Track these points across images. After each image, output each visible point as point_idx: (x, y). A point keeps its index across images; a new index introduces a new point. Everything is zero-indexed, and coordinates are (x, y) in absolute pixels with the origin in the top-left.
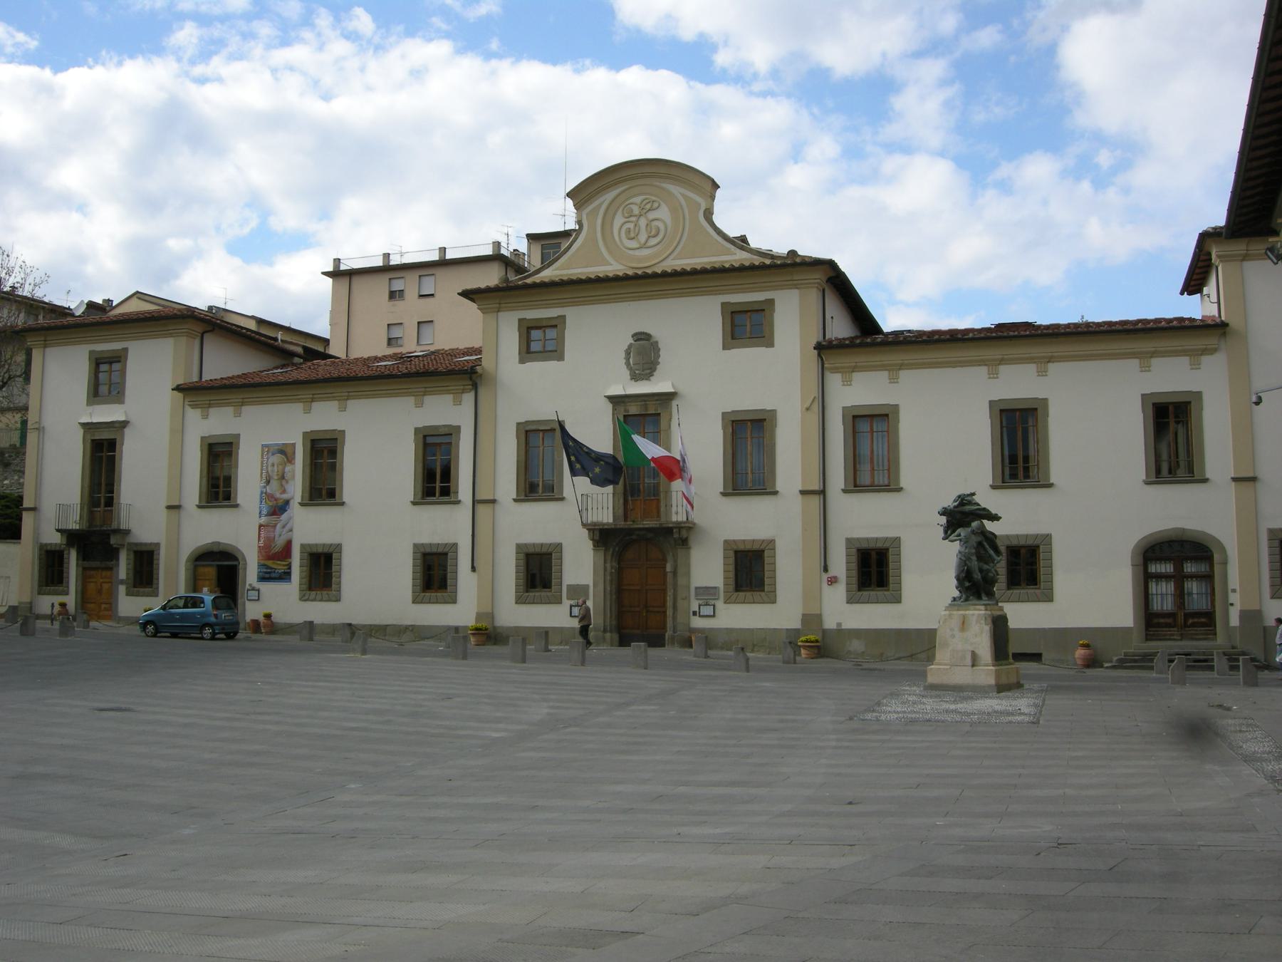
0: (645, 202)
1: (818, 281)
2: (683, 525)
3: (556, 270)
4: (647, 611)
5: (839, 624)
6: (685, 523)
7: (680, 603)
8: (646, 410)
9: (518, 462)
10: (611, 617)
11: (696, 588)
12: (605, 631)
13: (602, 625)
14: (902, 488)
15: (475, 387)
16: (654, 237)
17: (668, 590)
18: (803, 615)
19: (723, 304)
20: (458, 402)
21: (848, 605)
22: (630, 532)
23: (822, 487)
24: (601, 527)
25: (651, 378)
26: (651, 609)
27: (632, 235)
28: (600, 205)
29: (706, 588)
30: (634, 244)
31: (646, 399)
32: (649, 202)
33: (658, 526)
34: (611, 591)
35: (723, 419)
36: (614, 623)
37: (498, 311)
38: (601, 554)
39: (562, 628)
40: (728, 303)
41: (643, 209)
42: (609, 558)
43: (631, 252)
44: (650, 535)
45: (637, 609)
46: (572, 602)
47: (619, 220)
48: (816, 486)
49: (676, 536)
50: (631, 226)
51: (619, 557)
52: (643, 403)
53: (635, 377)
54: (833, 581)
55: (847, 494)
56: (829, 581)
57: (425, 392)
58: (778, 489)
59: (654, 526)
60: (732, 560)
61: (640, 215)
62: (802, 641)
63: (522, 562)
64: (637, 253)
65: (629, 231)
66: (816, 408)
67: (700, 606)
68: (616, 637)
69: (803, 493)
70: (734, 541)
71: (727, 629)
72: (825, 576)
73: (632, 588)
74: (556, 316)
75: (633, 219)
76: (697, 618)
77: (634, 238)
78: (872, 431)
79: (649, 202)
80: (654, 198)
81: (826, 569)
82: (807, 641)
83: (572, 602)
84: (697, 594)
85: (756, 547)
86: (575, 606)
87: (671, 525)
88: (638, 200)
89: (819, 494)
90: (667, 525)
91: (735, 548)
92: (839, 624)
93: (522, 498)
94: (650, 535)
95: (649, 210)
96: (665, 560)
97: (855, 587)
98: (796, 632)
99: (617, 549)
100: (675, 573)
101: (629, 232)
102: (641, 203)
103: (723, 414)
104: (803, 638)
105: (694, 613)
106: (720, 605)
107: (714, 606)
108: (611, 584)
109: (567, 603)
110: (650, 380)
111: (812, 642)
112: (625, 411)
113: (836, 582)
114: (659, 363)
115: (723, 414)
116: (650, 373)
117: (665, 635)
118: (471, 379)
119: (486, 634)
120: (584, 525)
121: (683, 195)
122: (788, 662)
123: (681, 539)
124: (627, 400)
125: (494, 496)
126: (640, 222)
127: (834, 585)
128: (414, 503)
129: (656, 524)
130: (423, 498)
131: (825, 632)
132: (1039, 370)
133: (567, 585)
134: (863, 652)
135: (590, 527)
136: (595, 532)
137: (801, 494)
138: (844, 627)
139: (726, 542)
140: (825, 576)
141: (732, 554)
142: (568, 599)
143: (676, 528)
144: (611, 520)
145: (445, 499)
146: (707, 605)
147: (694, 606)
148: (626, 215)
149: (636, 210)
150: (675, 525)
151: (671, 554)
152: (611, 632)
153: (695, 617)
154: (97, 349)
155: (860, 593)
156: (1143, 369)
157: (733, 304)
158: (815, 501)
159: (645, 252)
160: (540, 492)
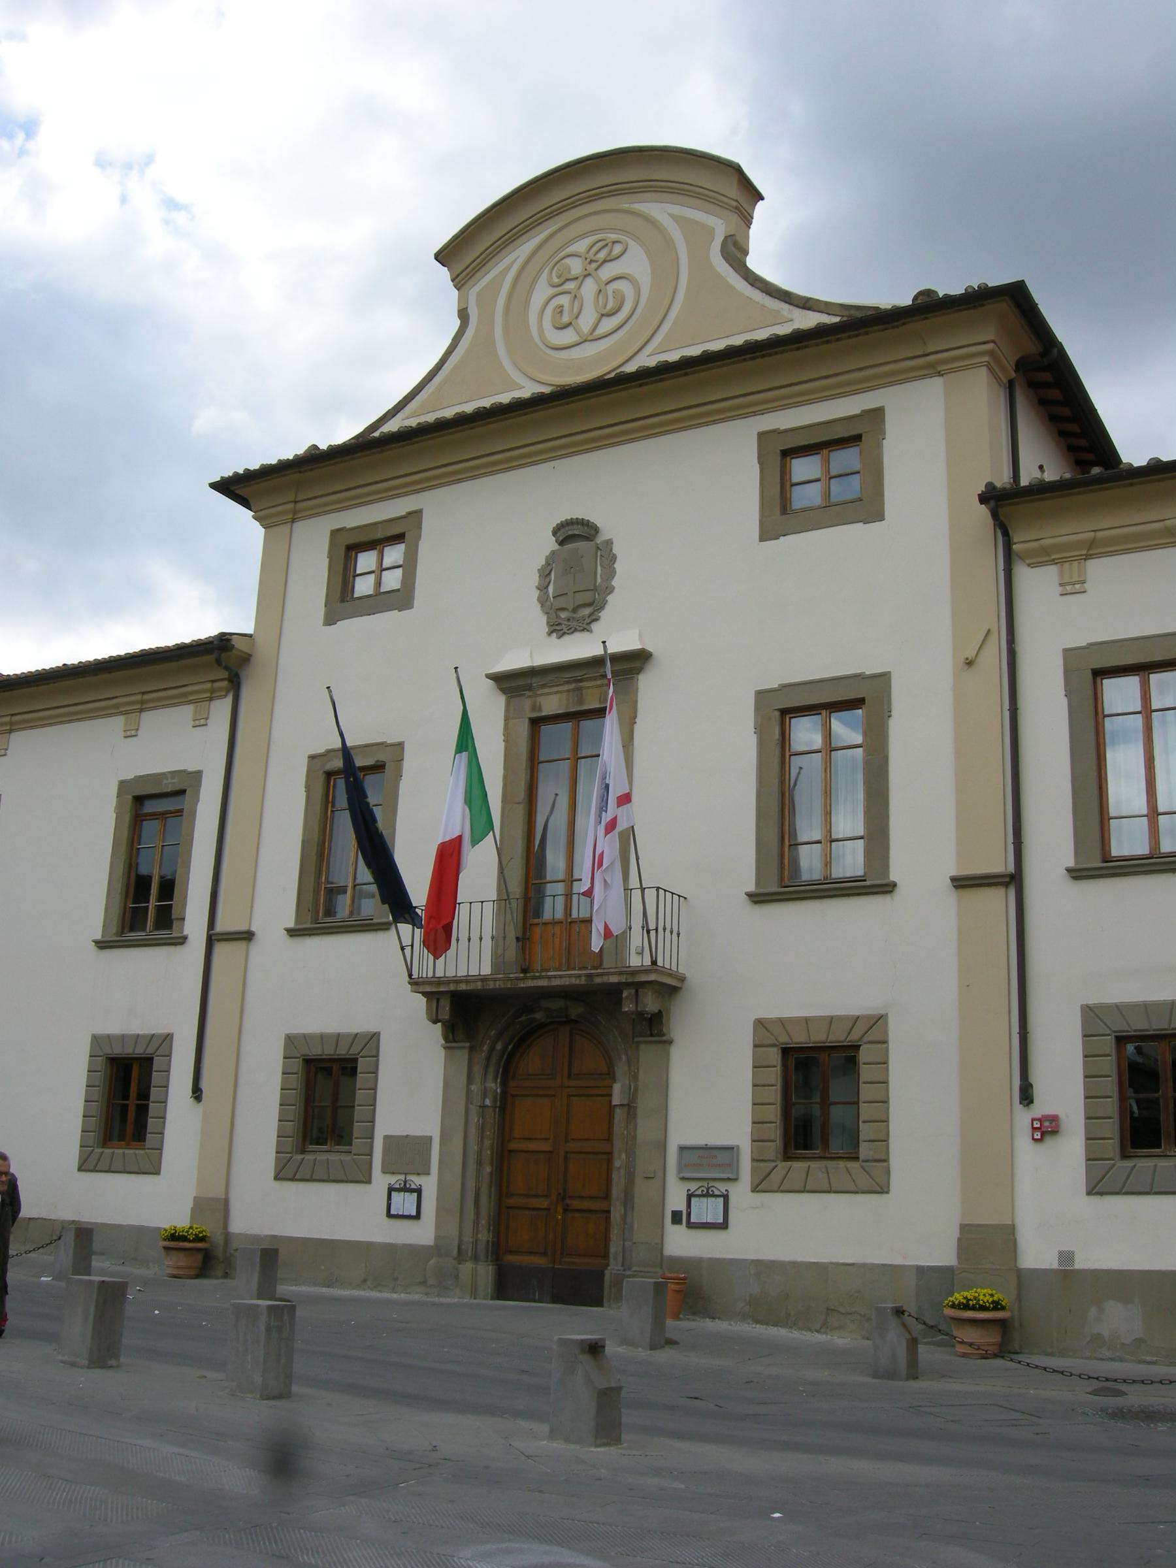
0: (594, 249)
1: (991, 346)
2: (643, 978)
3: (408, 418)
4: (566, 1210)
5: (1066, 1257)
6: (647, 971)
7: (641, 1187)
8: (581, 700)
9: (305, 843)
10: (477, 1220)
11: (682, 1149)
12: (461, 1256)
13: (456, 1243)
14: (894, 885)
15: (235, 684)
16: (609, 315)
17: (616, 1155)
18: (964, 1228)
19: (763, 436)
20: (201, 722)
21: (1092, 1198)
22: (528, 1000)
23: (1011, 868)
24: (452, 987)
25: (594, 626)
26: (575, 1204)
27: (566, 319)
28: (509, 268)
29: (706, 1148)
30: (569, 337)
31: (577, 674)
32: (607, 245)
33: (583, 981)
34: (480, 1152)
35: (758, 707)
36: (484, 1236)
37: (293, 521)
38: (463, 1056)
39: (369, 1245)
40: (774, 431)
41: (591, 261)
42: (478, 1069)
43: (563, 355)
44: (576, 1010)
45: (545, 1203)
46: (393, 1180)
47: (542, 291)
48: (1001, 864)
49: (628, 1007)
50: (565, 300)
51: (507, 1068)
52: (573, 686)
53: (558, 628)
54: (1046, 1129)
55: (104, 950)
56: (1034, 1129)
57: (212, 691)
58: (893, 877)
59: (574, 981)
60: (774, 1075)
61: (586, 276)
62: (953, 1306)
63: (295, 1081)
64: (576, 354)
65: (560, 310)
66: (993, 659)
67: (689, 1197)
68: (486, 1273)
69: (962, 883)
70: (782, 1022)
71: (757, 1263)
72: (1023, 1118)
73: (532, 1146)
74: (404, 513)
75: (571, 286)
76: (682, 1229)
77: (569, 324)
78: (1147, 711)
79: (607, 245)
80: (613, 237)
81: (1026, 1096)
82: (966, 1306)
83: (393, 1180)
84: (681, 1166)
85: (837, 1036)
86: (399, 1190)
87: (614, 979)
88: (581, 246)
89: (1006, 885)
90: (605, 979)
91: (784, 1039)
92: (1066, 1257)
93: (308, 925)
94: (576, 1010)
95: (605, 261)
96: (611, 1075)
97: (1112, 1146)
98: (943, 1277)
99: (499, 1046)
100: (630, 1108)
101: (561, 312)
102: (588, 252)
103: (760, 694)
104: (958, 1297)
105: (677, 1217)
106: (741, 1193)
107: (726, 1197)
108: (482, 1137)
109: (381, 1181)
110: (590, 631)
111: (983, 1308)
112: (535, 708)
113: (1055, 1132)
114: (610, 590)
115: (760, 694)
116: (590, 616)
117: (604, 1275)
118: (219, 662)
119: (198, 1250)
120: (416, 984)
121: (675, 218)
122: (891, 1374)
123: (641, 1015)
124: (535, 681)
125: (250, 927)
126: (583, 290)
127: (1049, 1141)
128: (102, 945)
129: (579, 976)
130: (121, 932)
131: (1022, 1277)
132: (1067, 580)
133: (386, 1137)
134: (1140, 1341)
135: (428, 989)
136: (442, 1002)
137: (957, 887)
138: (1080, 1264)
139: (760, 1024)
140: (1023, 1118)
141: (774, 1056)
142: (385, 1171)
143: (628, 985)
144: (486, 970)
145: (163, 934)
146: (707, 1195)
147: (676, 1199)
148: (556, 280)
149: (576, 266)
150: (623, 979)
151: (624, 1057)
152: (475, 1258)
153: (676, 1227)
154: (783, 427)
155: (1128, 1164)
156: (1069, 588)
157: (786, 431)
158: (998, 901)
159: (591, 349)
160: (148, 930)
